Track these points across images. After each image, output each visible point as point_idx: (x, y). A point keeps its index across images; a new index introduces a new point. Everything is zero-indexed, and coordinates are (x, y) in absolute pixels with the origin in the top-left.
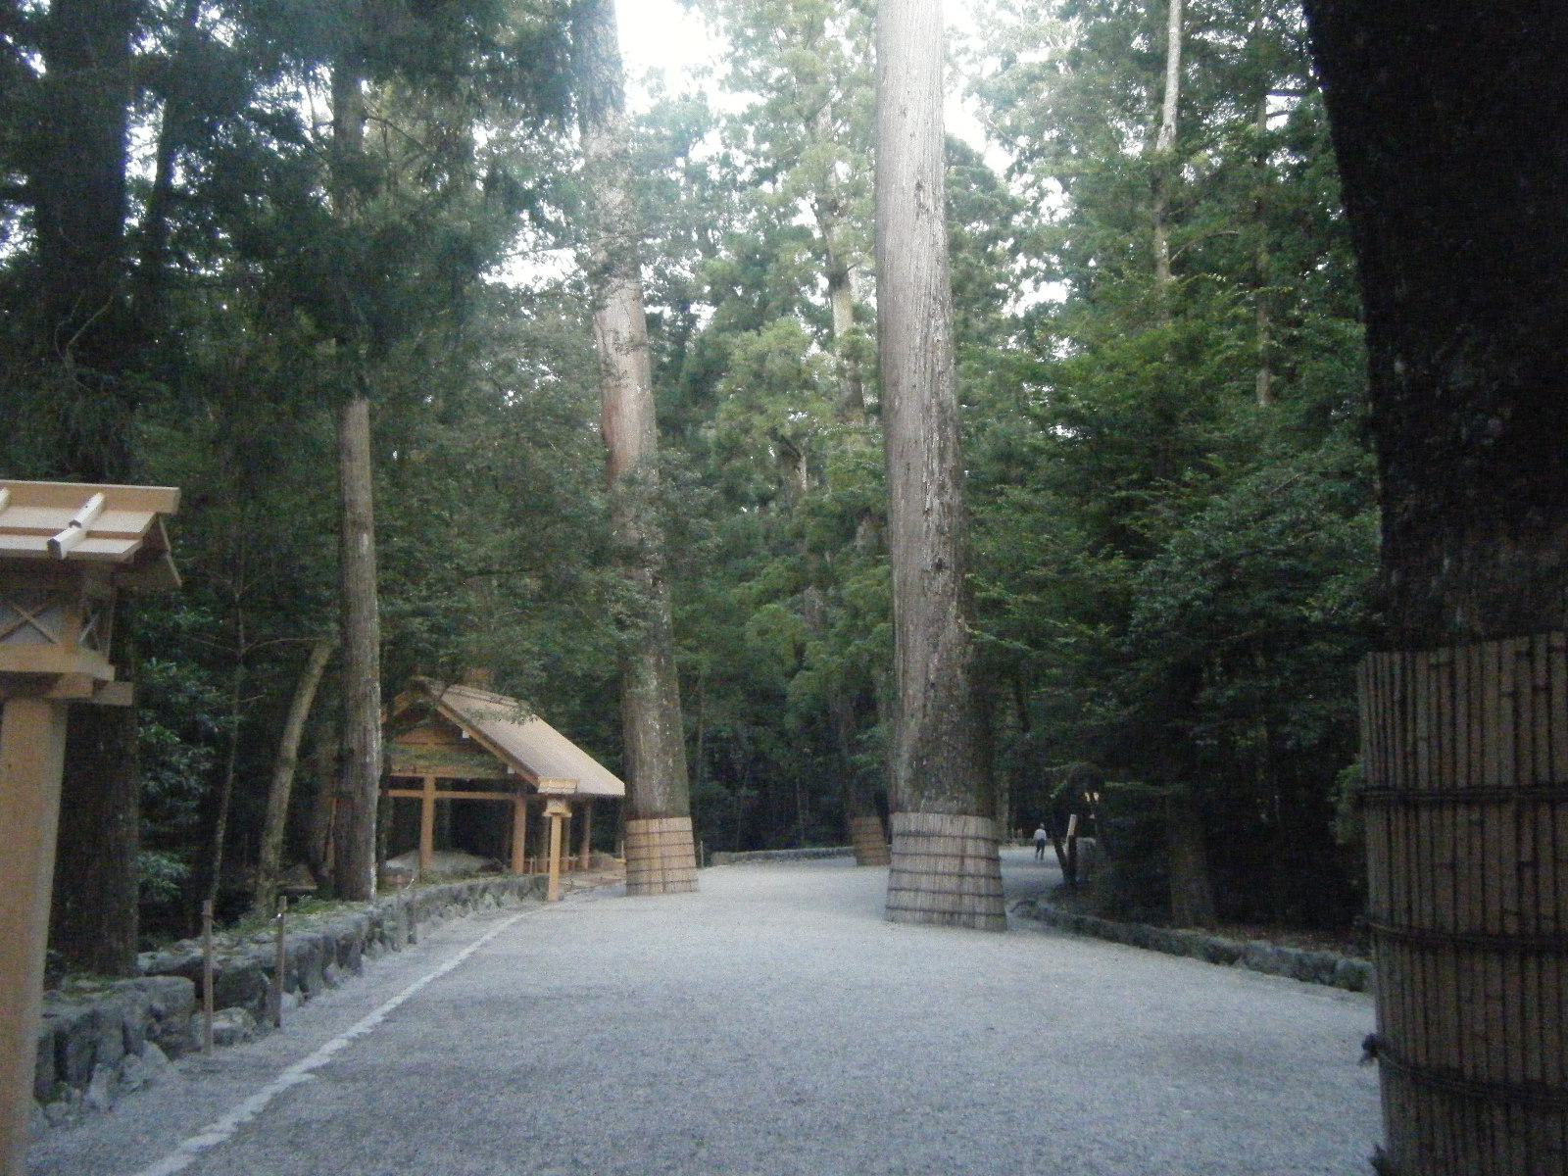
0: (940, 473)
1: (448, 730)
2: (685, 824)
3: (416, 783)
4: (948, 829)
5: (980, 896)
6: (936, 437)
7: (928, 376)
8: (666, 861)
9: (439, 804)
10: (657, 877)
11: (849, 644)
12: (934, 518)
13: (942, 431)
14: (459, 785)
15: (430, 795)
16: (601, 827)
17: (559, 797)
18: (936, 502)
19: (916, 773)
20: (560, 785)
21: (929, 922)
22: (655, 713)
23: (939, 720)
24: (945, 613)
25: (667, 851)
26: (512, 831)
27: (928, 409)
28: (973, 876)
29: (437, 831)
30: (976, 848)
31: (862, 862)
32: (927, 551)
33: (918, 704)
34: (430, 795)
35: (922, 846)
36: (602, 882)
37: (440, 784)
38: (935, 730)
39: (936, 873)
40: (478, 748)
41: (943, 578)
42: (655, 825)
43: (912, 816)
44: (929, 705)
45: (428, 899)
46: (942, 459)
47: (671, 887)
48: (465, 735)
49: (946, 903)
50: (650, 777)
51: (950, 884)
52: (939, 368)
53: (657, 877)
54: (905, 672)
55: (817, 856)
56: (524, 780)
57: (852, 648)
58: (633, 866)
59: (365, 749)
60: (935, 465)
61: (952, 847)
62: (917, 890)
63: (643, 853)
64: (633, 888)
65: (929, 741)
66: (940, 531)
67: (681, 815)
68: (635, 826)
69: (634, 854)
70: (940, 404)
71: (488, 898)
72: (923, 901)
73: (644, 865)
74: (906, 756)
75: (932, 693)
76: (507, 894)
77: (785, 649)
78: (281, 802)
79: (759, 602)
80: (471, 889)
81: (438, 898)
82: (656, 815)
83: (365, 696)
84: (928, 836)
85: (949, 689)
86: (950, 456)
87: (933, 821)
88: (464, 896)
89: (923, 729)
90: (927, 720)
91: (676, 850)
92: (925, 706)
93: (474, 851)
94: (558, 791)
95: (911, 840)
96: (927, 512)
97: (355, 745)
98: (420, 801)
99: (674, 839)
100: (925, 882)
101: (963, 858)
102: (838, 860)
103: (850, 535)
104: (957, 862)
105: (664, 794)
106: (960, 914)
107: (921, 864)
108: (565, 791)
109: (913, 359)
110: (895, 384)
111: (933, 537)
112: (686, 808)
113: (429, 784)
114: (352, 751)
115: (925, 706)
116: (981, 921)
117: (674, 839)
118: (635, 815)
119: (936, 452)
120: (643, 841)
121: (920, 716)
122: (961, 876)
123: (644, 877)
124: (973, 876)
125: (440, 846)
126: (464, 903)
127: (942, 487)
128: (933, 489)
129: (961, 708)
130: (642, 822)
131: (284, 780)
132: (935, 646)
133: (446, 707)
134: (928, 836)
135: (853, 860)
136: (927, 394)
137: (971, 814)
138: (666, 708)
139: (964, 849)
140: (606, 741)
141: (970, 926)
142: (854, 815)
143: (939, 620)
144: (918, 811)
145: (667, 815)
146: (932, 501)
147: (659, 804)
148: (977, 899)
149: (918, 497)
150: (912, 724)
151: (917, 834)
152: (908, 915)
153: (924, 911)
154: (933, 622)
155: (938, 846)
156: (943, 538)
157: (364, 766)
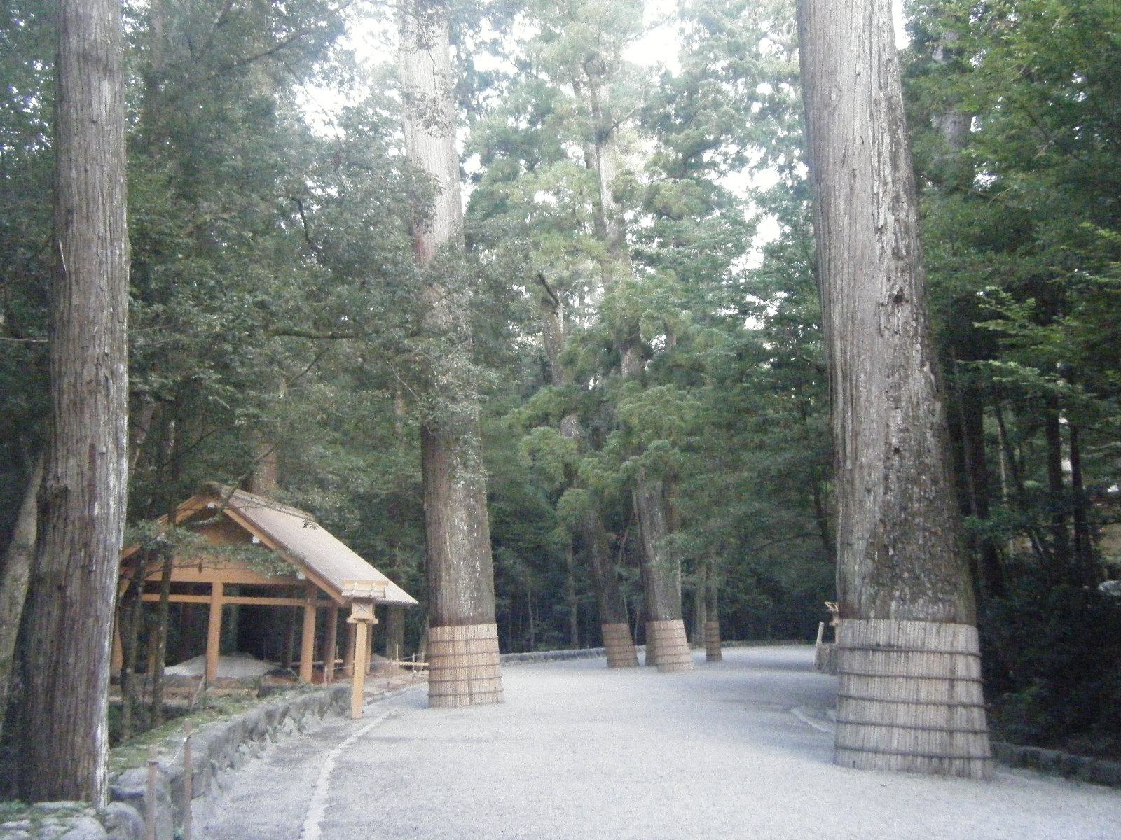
0: (894, 182)
1: (235, 532)
2: (491, 630)
3: (205, 589)
4: (933, 642)
5: (975, 733)
6: (887, 139)
7: (875, 64)
8: (473, 670)
9: (226, 611)
10: (463, 688)
11: (624, 459)
12: (888, 237)
13: (893, 133)
14: (246, 590)
15: (217, 602)
16: (406, 633)
17: (366, 601)
18: (891, 219)
19: (879, 565)
20: (368, 588)
21: (910, 770)
22: (463, 514)
23: (905, 495)
24: (907, 359)
25: (474, 660)
26: (299, 643)
27: (877, 103)
28: (965, 706)
29: (223, 641)
30: (968, 667)
31: (612, 664)
32: (881, 280)
33: (877, 475)
34: (217, 602)
35: (898, 665)
36: (389, 687)
37: (229, 589)
38: (903, 509)
39: (918, 703)
40: (273, 549)
41: (902, 314)
42: (461, 632)
43: (882, 624)
44: (892, 477)
45: (215, 749)
46: (895, 168)
47: (477, 699)
48: (256, 540)
49: (932, 743)
50: (456, 581)
51: (937, 717)
52: (885, 57)
53: (463, 688)
54: (856, 435)
55: (563, 658)
56: (315, 584)
57: (628, 463)
58: (437, 677)
59: (91, 492)
60: (888, 171)
61: (937, 666)
62: (892, 726)
63: (449, 662)
64: (435, 699)
65: (896, 527)
66: (896, 254)
67: (488, 622)
68: (438, 633)
69: (438, 663)
70: (889, 99)
71: (289, 723)
72: (900, 740)
73: (449, 675)
74: (860, 546)
75: (896, 461)
76: (308, 716)
77: (556, 469)
78: (13, 604)
79: (528, 427)
80: (270, 715)
81: (227, 741)
82: (461, 622)
83: (97, 386)
84: (906, 651)
85: (919, 455)
86: (902, 164)
87: (912, 632)
88: (262, 726)
89: (886, 506)
90: (890, 497)
91: (482, 659)
92: (886, 478)
93: (259, 656)
94: (365, 595)
95: (880, 657)
96: (880, 230)
97: (70, 482)
98: (206, 608)
99: (481, 646)
100: (902, 715)
101: (952, 681)
102: (575, 662)
103: (616, 363)
104: (944, 686)
105: (472, 598)
106: (951, 758)
107: (899, 689)
108: (373, 595)
109: (855, 42)
110: (832, 73)
111: (888, 261)
112: (492, 614)
113: (218, 590)
114: (65, 492)
115: (886, 478)
116: (977, 767)
117: (481, 646)
118: (438, 622)
119: (886, 157)
120: (449, 649)
121: (881, 491)
122: (951, 707)
123: (449, 688)
124: (965, 706)
125: (225, 651)
126: (262, 736)
127: (896, 199)
128: (886, 201)
129: (935, 482)
130: (448, 629)
131: (19, 572)
132: (897, 400)
133: (236, 510)
134: (906, 651)
135: (603, 660)
136: (875, 85)
137: (961, 623)
138: (474, 509)
139: (953, 671)
140: (382, 554)
141: (964, 774)
142: (606, 622)
143: (899, 368)
144: (887, 617)
145: (474, 621)
146: (886, 217)
147: (466, 609)
148: (971, 737)
149: (868, 211)
150: (869, 504)
151: (889, 648)
152: (880, 760)
153: (904, 754)
154: (893, 369)
155: (919, 665)
156: (900, 263)
157: (90, 523)
